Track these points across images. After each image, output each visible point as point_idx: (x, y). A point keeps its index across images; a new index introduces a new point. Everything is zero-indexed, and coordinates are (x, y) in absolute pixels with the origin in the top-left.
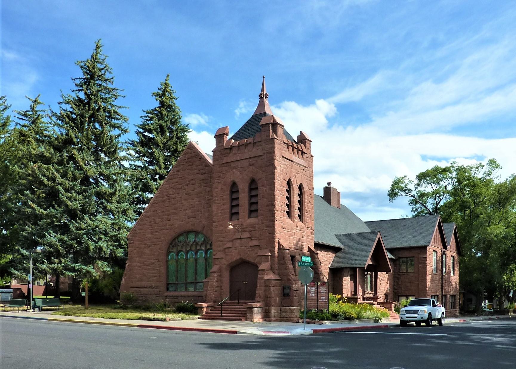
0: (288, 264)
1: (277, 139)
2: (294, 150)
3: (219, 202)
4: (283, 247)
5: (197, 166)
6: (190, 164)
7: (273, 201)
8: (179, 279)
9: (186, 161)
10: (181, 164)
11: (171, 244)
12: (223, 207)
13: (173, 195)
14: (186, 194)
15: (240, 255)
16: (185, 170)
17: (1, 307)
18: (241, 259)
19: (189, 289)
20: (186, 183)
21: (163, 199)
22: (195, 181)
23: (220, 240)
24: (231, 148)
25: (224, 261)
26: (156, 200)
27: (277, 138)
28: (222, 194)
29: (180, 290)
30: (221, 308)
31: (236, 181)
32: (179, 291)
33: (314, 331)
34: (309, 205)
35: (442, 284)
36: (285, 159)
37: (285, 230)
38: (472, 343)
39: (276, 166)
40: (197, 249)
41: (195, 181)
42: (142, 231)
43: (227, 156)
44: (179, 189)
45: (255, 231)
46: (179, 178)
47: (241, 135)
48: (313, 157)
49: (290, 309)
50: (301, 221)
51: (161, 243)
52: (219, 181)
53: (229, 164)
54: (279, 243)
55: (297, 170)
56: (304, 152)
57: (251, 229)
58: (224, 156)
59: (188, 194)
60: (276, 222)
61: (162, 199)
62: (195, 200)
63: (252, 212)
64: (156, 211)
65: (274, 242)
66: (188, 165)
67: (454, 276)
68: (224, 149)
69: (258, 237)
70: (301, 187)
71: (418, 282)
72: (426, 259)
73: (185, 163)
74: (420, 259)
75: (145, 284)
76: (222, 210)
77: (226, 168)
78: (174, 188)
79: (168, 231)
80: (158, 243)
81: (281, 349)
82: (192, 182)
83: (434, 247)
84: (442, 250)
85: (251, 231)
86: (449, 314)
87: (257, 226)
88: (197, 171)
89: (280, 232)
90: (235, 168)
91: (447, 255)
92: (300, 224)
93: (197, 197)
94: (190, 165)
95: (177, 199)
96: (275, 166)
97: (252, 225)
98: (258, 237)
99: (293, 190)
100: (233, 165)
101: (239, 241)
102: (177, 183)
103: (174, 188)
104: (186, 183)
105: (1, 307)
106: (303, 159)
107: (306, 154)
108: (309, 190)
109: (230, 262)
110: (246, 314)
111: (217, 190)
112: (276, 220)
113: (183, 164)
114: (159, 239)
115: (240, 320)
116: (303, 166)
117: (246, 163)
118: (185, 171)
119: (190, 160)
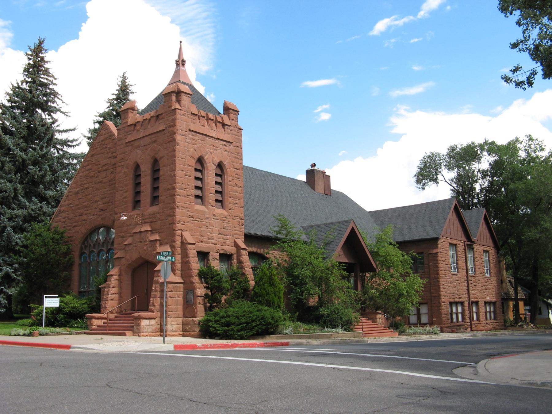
0: (191, 262)
1: (181, 110)
2: (209, 122)
3: (121, 189)
4: (186, 240)
5: (110, 148)
6: (104, 146)
7: (174, 184)
9: (100, 144)
11: (83, 243)
14: (99, 183)
15: (140, 252)
16: (99, 154)
18: (141, 257)
22: (107, 167)
24: (135, 125)
25: (123, 261)
26: (71, 192)
27: (181, 109)
28: (125, 179)
30: (362, 325)
31: (139, 162)
33: (176, 347)
34: (236, 188)
35: (468, 287)
36: (192, 133)
37: (192, 219)
38: (280, 363)
39: (178, 141)
41: (107, 167)
43: (130, 134)
44: (92, 176)
45: (156, 221)
46: (93, 164)
48: (242, 130)
49: (193, 320)
52: (122, 163)
53: (132, 143)
54: (182, 236)
55: (214, 146)
56: (225, 123)
58: (128, 133)
60: (176, 209)
62: (107, 189)
63: (155, 199)
64: (70, 204)
65: (174, 235)
66: (101, 148)
67: (491, 277)
68: (128, 126)
70: (220, 166)
71: (429, 286)
72: (437, 255)
74: (430, 255)
76: (124, 198)
77: (130, 148)
78: (87, 176)
79: (80, 227)
81: (451, 376)
82: (104, 168)
83: (450, 239)
84: (464, 244)
85: (151, 222)
86: (484, 327)
87: (158, 216)
88: (110, 155)
89: (184, 222)
90: (138, 147)
91: (475, 250)
92: (220, 211)
93: (109, 186)
94: (103, 149)
96: (177, 141)
97: (152, 215)
99: (207, 170)
100: (136, 144)
101: (139, 235)
102: (91, 171)
103: (87, 176)
106: (224, 132)
107: (229, 126)
108: (235, 170)
109: (129, 262)
110: (133, 327)
111: (120, 175)
112: (178, 207)
115: (124, 335)
117: (147, 140)
118: (99, 156)
119: (104, 142)
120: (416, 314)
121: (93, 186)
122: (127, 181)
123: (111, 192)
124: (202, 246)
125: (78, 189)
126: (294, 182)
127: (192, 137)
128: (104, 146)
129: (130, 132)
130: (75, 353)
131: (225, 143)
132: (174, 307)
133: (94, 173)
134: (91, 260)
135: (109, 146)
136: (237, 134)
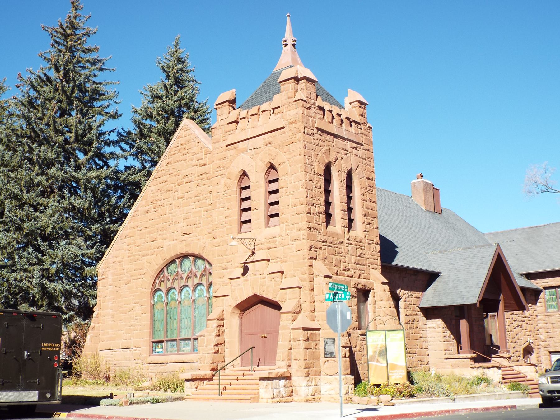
6: (185, 152)
8: (169, 334)
9: (178, 148)
10: (172, 153)
12: (228, 212)
13: (160, 202)
17: (559, 192)
19: (184, 349)
20: (179, 181)
21: (146, 208)
23: (224, 266)
29: (171, 352)
32: (169, 353)
40: (180, 286)
42: (118, 259)
47: (254, 101)
50: (558, 368)
51: (143, 276)
57: (270, 245)
58: (229, 133)
59: (182, 198)
61: (145, 208)
69: (280, 258)
73: (177, 152)
75: (120, 343)
76: (226, 217)
77: (233, 152)
80: (139, 277)
82: (187, 179)
87: (278, 239)
90: (244, 150)
94: (184, 154)
95: (166, 206)
98: (280, 258)
104: (179, 181)
105: (559, 192)
113: (174, 153)
114: (141, 270)
116: (353, 141)
120: (218, 384)
121: (170, 202)
122: (229, 195)
123: (198, 209)
124: (337, 279)
125: (148, 207)
126: (399, 197)
127: (319, 137)
128: (185, 152)
129: (232, 132)
130: (519, 411)
131: (355, 145)
132: (311, 361)
133: (171, 185)
134: (170, 299)
135: (192, 151)
136: (367, 133)
